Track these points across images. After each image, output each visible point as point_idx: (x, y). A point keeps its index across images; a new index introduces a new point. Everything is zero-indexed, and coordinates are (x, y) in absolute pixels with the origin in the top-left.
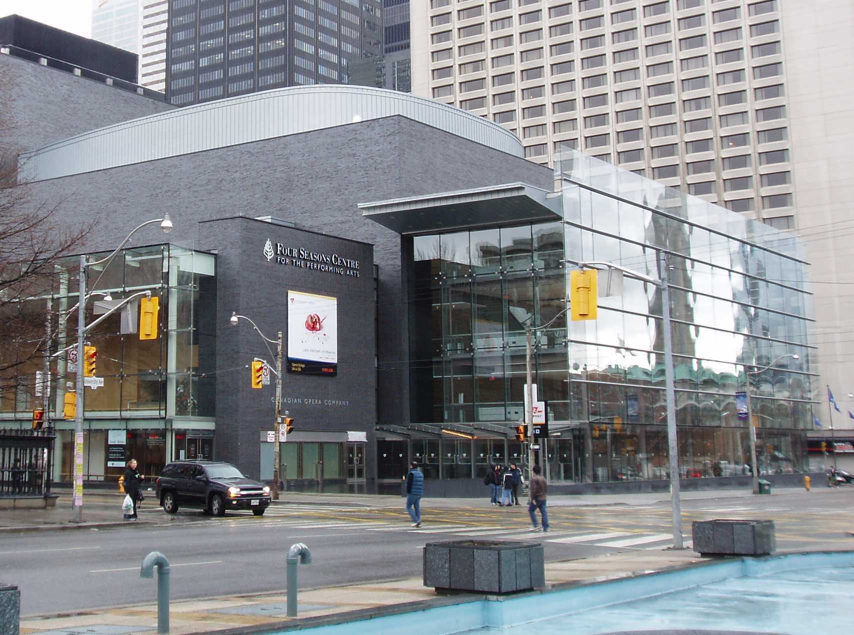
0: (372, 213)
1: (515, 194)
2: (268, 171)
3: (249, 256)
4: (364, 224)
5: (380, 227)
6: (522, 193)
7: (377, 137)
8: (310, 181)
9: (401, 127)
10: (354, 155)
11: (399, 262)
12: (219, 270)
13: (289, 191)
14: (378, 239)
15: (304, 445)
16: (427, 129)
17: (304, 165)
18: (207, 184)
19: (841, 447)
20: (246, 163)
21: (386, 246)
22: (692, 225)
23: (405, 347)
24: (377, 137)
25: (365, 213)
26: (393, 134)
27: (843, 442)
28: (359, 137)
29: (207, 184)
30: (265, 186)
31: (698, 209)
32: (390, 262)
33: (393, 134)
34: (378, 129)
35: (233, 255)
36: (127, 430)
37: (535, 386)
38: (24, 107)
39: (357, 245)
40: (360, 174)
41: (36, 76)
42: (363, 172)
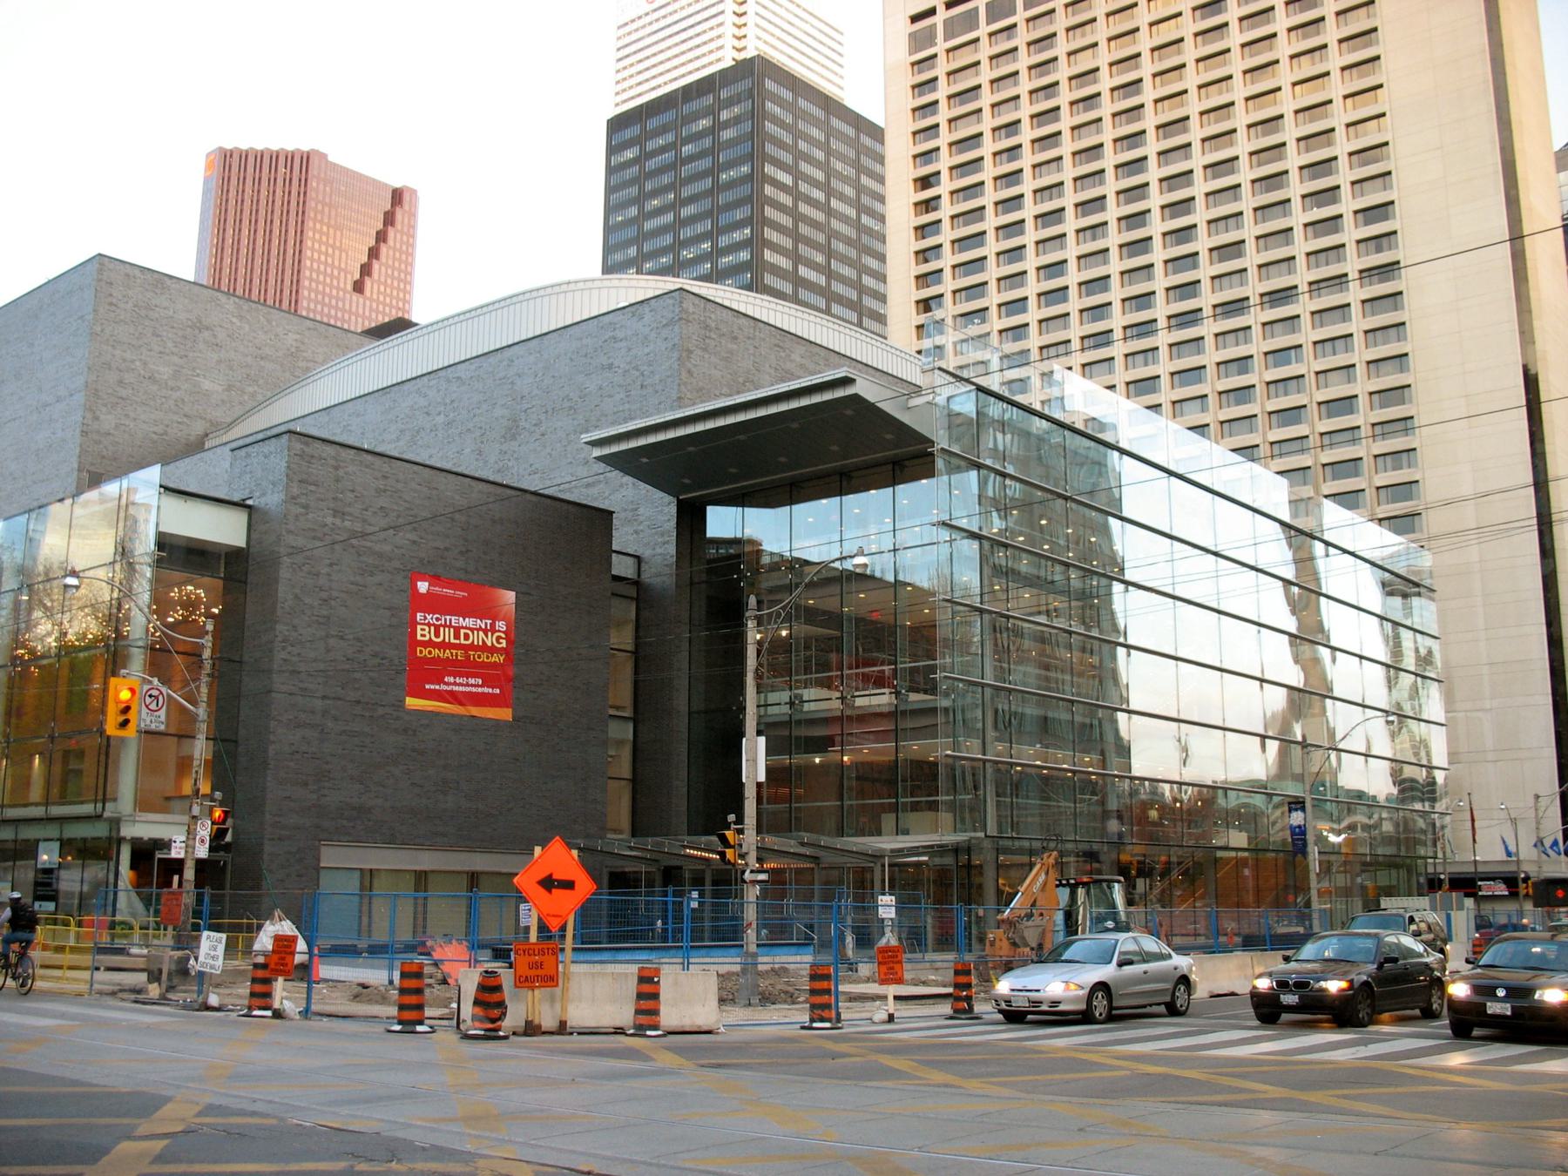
0: (607, 451)
1: (840, 393)
2: (484, 406)
3: (306, 507)
4: (621, 486)
5: (615, 475)
6: (849, 391)
7: (647, 330)
8: (543, 417)
9: (683, 310)
10: (610, 366)
11: (672, 549)
12: (253, 536)
13: (514, 438)
14: (641, 511)
15: (431, 877)
16: (743, 321)
17: (536, 392)
18: (398, 439)
19: (1489, 887)
20: (454, 396)
21: (644, 523)
22: (1327, 544)
23: (681, 702)
24: (647, 330)
25: (597, 452)
26: (671, 323)
27: (1493, 879)
28: (620, 334)
29: (398, 439)
30: (478, 434)
31: (1335, 519)
32: (659, 551)
33: (671, 323)
34: (648, 317)
35: (271, 499)
36: (60, 840)
37: (762, 740)
38: (219, 362)
39: (572, 509)
40: (617, 397)
41: (241, 318)
42: (622, 395)
